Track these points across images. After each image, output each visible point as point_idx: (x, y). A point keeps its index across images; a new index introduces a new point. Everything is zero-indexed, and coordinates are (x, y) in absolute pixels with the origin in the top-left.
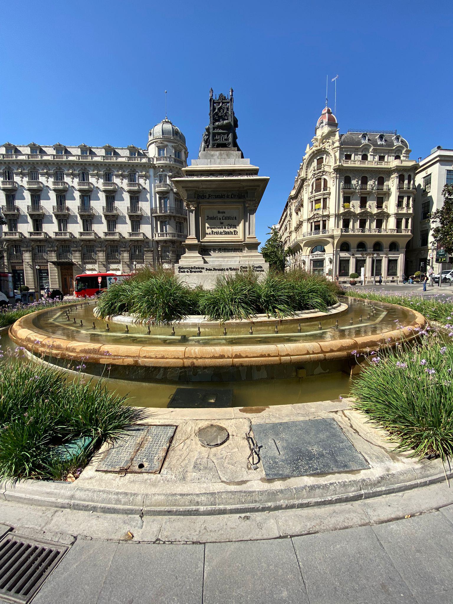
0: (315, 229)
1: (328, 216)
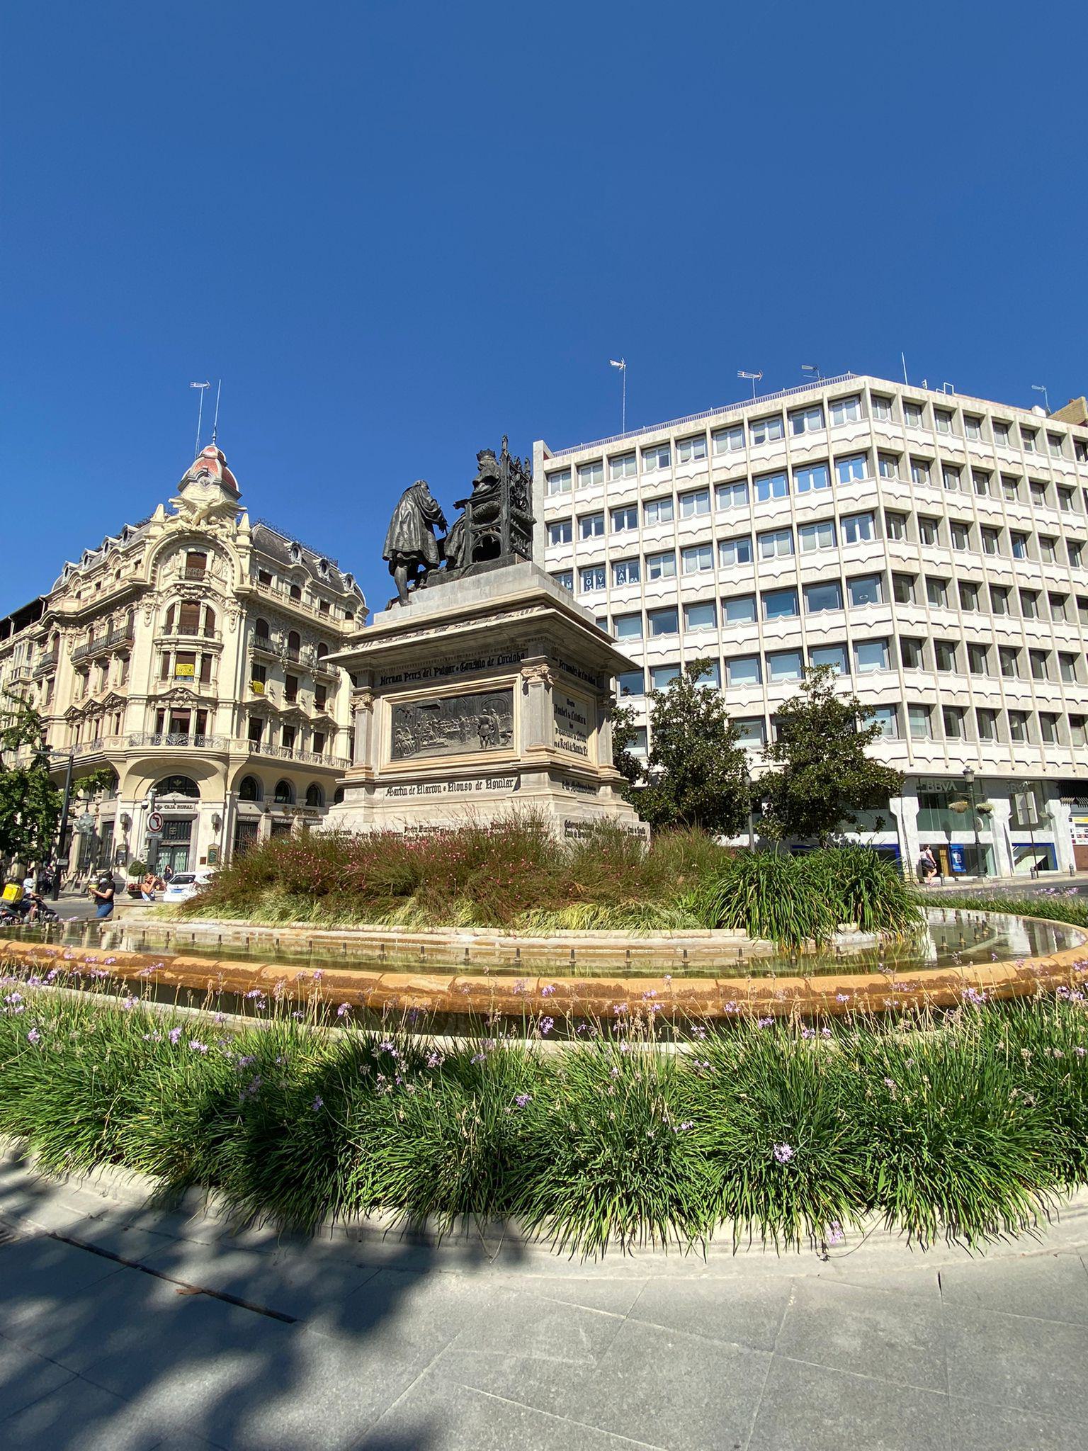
0: (172, 730)
1: (215, 703)
